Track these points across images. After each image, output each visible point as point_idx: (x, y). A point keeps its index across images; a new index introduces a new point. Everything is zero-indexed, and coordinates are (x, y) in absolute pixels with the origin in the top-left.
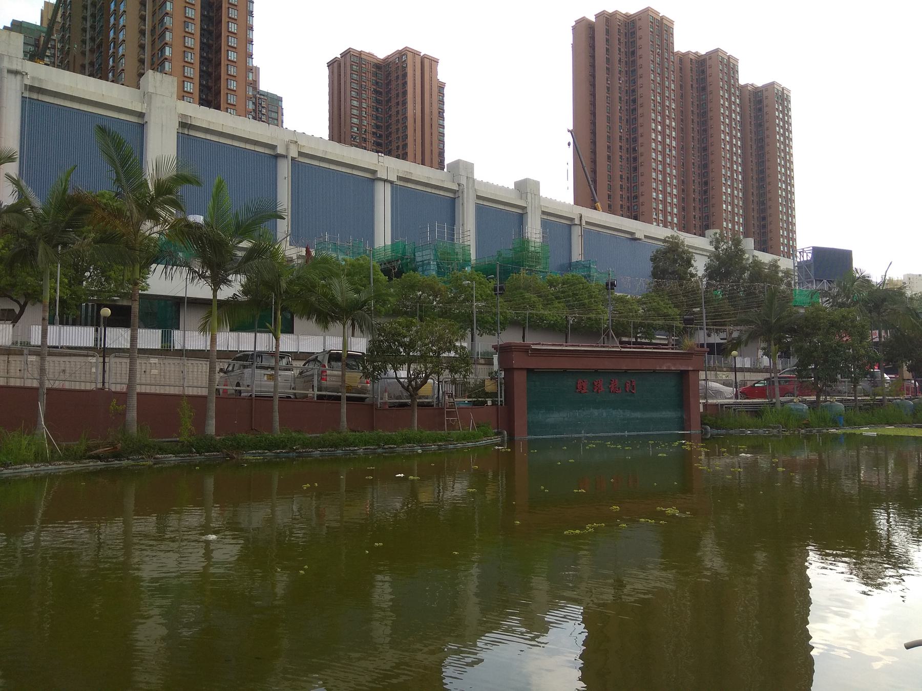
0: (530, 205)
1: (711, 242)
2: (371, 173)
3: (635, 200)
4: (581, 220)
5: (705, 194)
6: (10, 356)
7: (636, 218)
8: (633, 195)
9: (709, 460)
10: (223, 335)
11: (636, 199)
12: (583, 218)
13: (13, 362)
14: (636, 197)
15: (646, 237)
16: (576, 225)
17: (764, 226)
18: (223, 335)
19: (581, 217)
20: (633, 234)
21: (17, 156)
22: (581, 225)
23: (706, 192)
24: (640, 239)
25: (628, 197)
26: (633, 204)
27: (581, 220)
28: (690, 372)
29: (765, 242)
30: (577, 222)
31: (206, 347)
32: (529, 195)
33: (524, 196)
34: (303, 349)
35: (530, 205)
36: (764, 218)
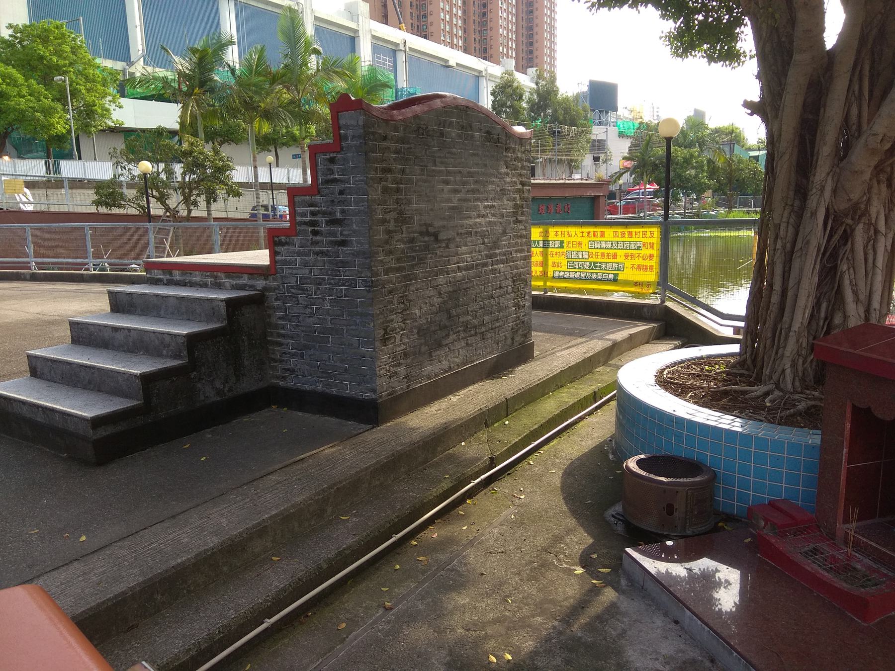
0: (361, 28)
1: (532, 79)
2: (353, 32)
3: (424, 19)
4: (405, 46)
5: (483, 16)
6: (48, 190)
7: (425, 37)
8: (422, 13)
9: (885, 172)
10: (28, 164)
11: (425, 18)
12: (407, 44)
13: (51, 195)
14: (425, 16)
15: (457, 64)
16: (401, 50)
17: (531, 52)
18: (28, 164)
19: (405, 43)
20: (447, 61)
21: (235, 39)
22: (405, 51)
23: (484, 14)
24: (452, 67)
25: (417, 16)
26: (422, 23)
27: (405, 46)
28: (601, 197)
29: (485, 51)
30: (402, 47)
31: (249, 180)
32: (360, 18)
33: (355, 18)
34: (90, 176)
35: (361, 28)
36: (531, 44)
